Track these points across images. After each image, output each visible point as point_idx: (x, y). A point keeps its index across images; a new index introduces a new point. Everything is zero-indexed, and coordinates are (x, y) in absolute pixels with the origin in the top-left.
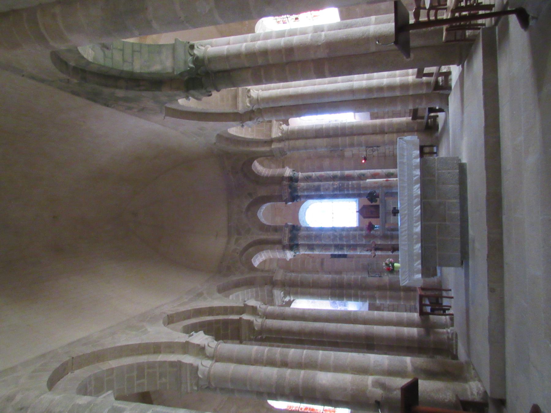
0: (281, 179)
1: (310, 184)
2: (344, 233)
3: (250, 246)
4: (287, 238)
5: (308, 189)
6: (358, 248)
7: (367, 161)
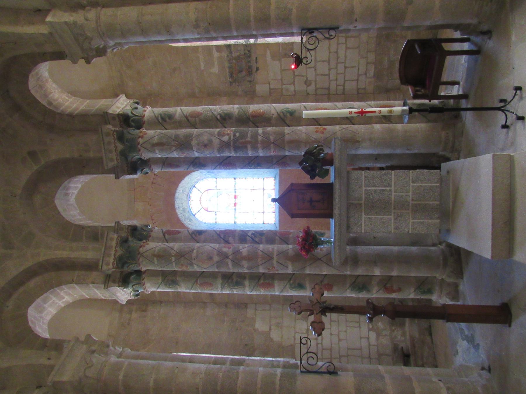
0: (105, 117)
1: (171, 132)
2: (245, 249)
3: (31, 273)
4: (111, 260)
5: (161, 145)
6: (276, 283)
7: (302, 67)
